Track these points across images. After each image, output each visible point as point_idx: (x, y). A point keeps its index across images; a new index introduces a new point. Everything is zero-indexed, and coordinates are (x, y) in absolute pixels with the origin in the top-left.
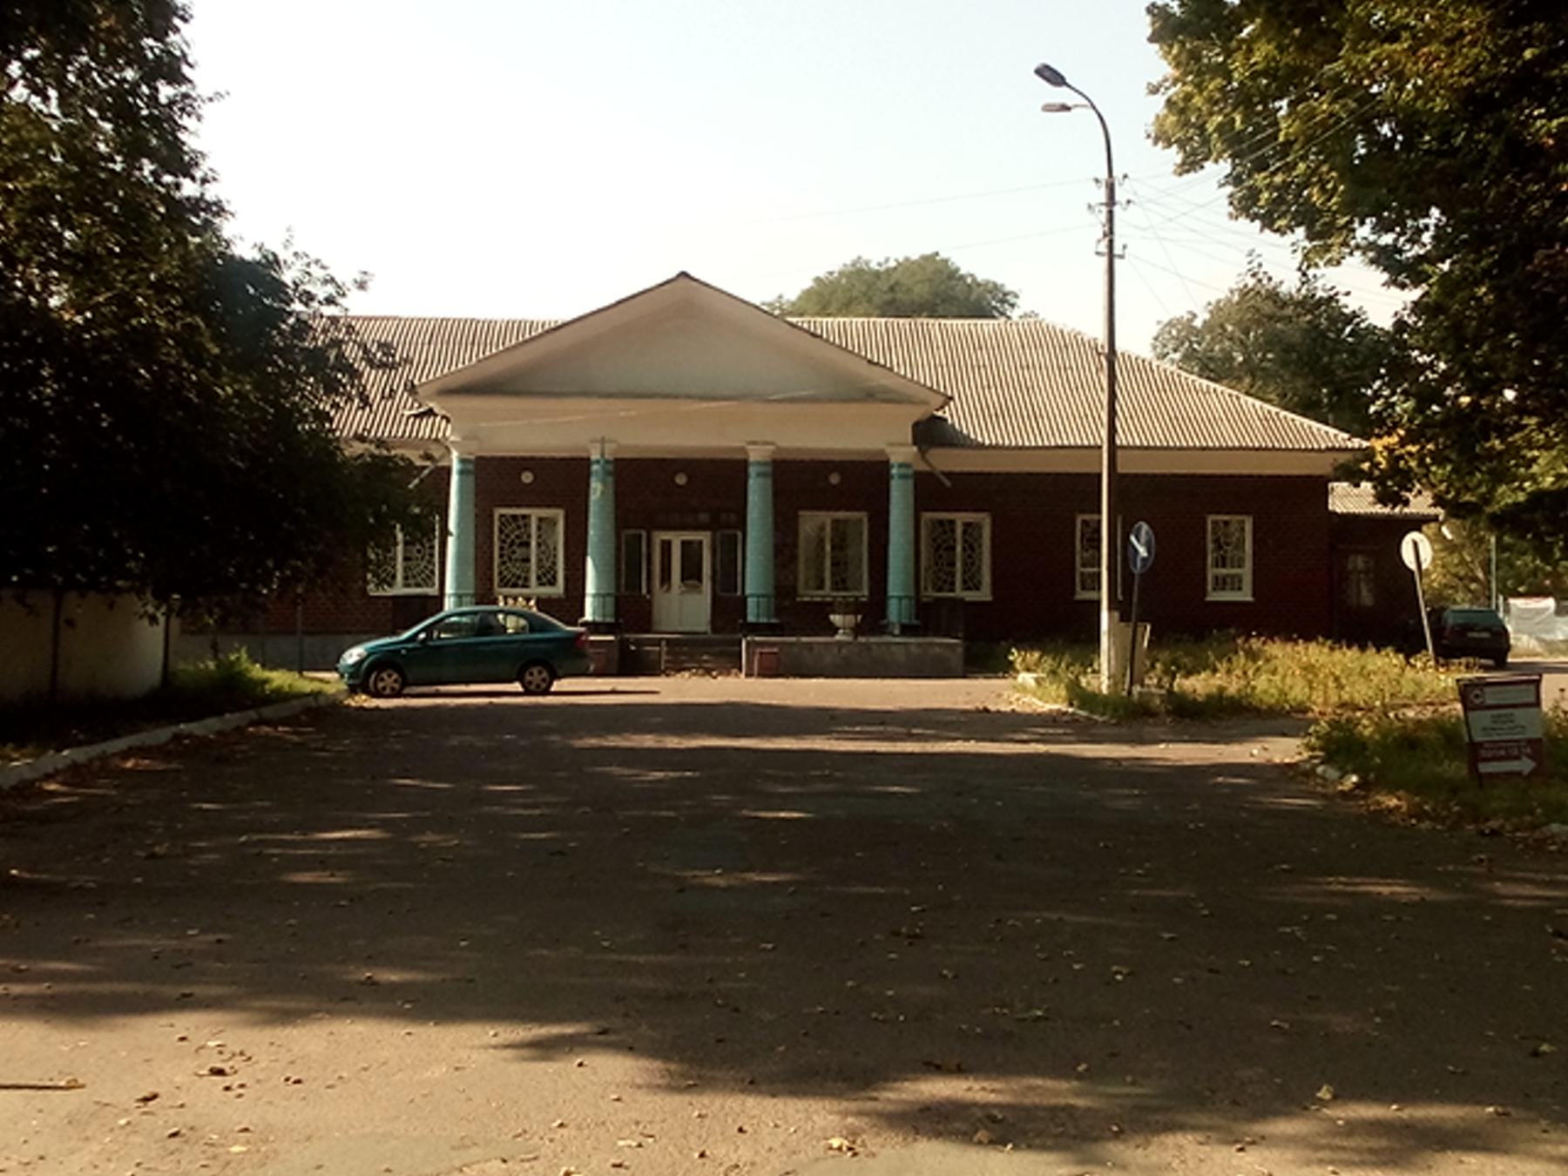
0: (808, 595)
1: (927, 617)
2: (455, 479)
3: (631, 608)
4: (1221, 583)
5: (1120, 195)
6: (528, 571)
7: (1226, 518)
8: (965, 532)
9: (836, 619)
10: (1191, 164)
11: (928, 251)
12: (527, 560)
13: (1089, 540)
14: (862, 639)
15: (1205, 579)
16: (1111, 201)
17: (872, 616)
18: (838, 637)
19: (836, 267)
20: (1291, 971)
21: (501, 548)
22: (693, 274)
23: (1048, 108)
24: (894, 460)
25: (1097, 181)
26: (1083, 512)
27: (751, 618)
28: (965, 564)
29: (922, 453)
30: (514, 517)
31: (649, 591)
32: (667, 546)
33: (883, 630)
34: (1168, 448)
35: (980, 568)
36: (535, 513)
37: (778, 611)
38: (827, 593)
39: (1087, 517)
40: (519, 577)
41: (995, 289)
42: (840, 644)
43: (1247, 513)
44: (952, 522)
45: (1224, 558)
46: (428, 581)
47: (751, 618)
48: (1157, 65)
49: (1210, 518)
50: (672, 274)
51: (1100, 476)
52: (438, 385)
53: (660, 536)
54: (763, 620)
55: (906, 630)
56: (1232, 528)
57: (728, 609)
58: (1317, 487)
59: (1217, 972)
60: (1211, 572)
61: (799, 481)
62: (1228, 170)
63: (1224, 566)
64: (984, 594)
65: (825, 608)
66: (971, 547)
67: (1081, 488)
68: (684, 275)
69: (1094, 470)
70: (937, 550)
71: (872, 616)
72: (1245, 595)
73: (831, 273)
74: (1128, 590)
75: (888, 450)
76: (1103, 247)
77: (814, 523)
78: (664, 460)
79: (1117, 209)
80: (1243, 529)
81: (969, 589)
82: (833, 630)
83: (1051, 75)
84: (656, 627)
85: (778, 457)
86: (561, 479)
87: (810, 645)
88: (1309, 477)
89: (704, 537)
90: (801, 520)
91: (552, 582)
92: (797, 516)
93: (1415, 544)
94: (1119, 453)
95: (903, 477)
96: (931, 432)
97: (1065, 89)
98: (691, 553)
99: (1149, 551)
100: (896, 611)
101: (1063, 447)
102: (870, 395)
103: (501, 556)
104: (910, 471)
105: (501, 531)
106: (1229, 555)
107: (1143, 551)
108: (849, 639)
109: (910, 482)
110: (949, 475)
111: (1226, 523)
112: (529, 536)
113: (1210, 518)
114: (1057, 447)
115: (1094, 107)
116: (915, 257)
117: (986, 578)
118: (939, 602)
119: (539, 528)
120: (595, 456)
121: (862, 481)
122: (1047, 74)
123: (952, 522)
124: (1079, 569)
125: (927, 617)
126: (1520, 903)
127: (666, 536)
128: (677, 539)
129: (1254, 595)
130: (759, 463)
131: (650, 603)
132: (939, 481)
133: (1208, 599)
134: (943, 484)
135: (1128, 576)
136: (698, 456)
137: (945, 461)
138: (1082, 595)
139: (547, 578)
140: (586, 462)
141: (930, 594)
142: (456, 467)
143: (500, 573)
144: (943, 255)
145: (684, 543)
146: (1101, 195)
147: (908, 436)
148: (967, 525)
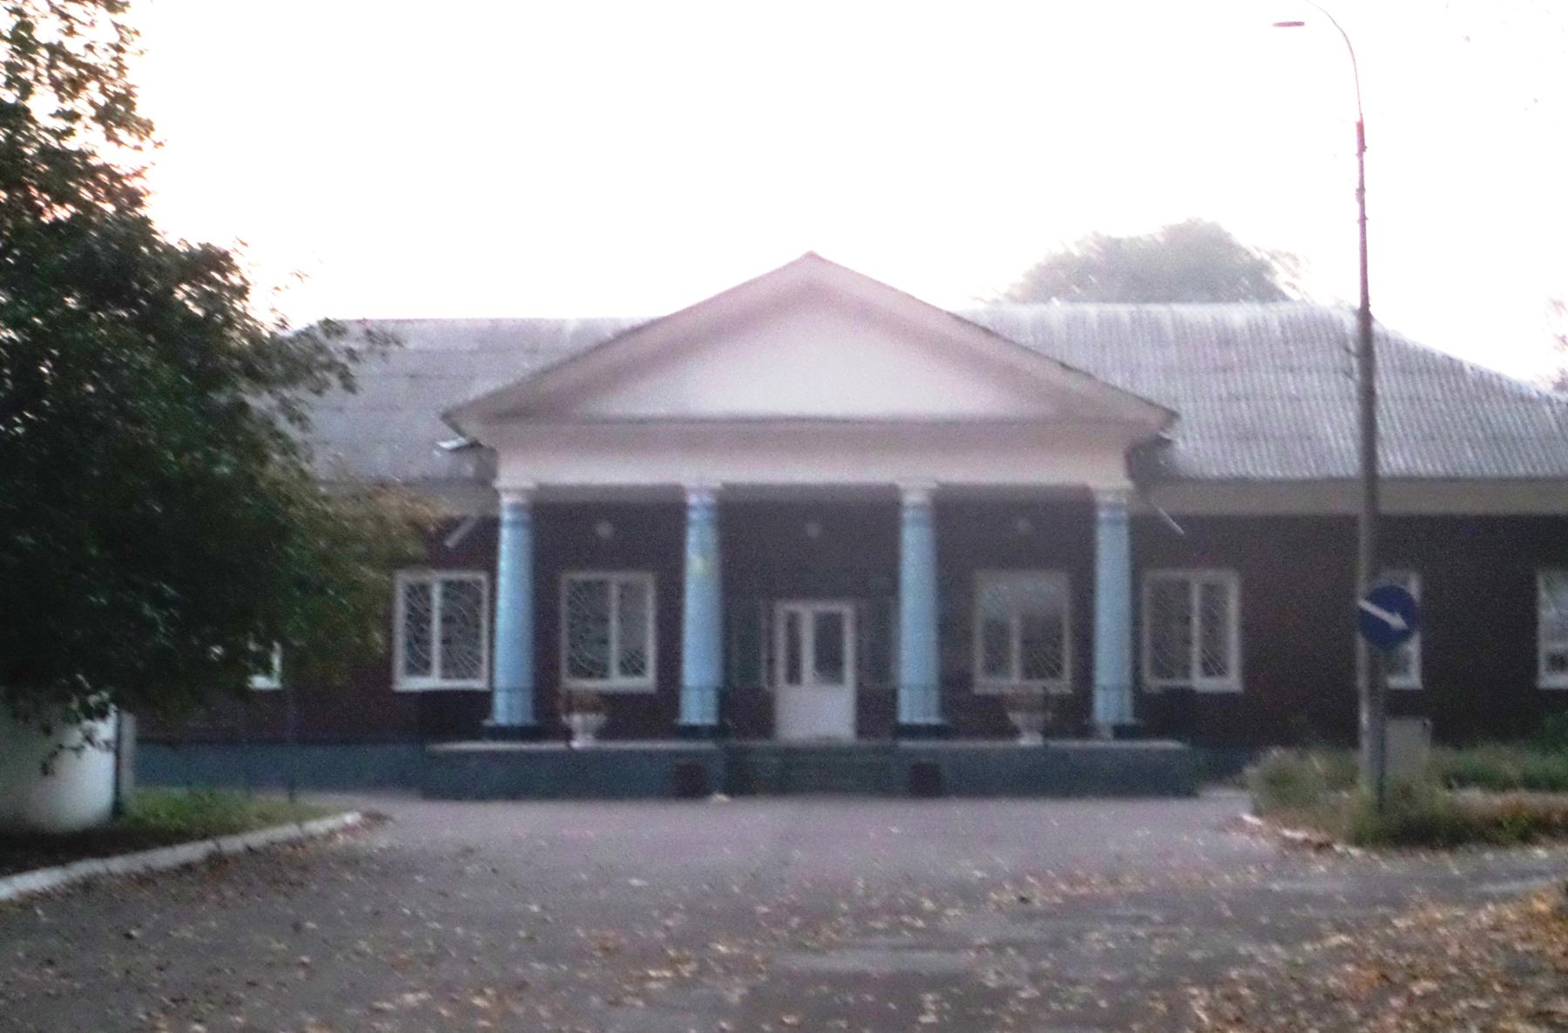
0: (985, 684)
1: (1162, 711)
2: (506, 534)
9: (1017, 718)
11: (1141, 212)
30: (587, 584)
31: (771, 682)
32: (793, 623)
37: (945, 707)
46: (472, 673)
53: (783, 608)
57: (875, 707)
61: (979, 532)
64: (1232, 682)
66: (1213, 620)
68: (811, 256)
77: (1009, 595)
82: (568, 734)
86: (647, 528)
89: (846, 610)
91: (1055, 671)
95: (1114, 522)
96: (1147, 456)
98: (829, 632)
100: (1110, 705)
109: (1124, 531)
110: (1185, 520)
117: (1234, 658)
118: (1170, 693)
126: (1147, 620)
127: (792, 607)
128: (807, 613)
132: (1166, 526)
139: (633, 665)
141: (1153, 683)
142: (506, 516)
143: (571, 659)
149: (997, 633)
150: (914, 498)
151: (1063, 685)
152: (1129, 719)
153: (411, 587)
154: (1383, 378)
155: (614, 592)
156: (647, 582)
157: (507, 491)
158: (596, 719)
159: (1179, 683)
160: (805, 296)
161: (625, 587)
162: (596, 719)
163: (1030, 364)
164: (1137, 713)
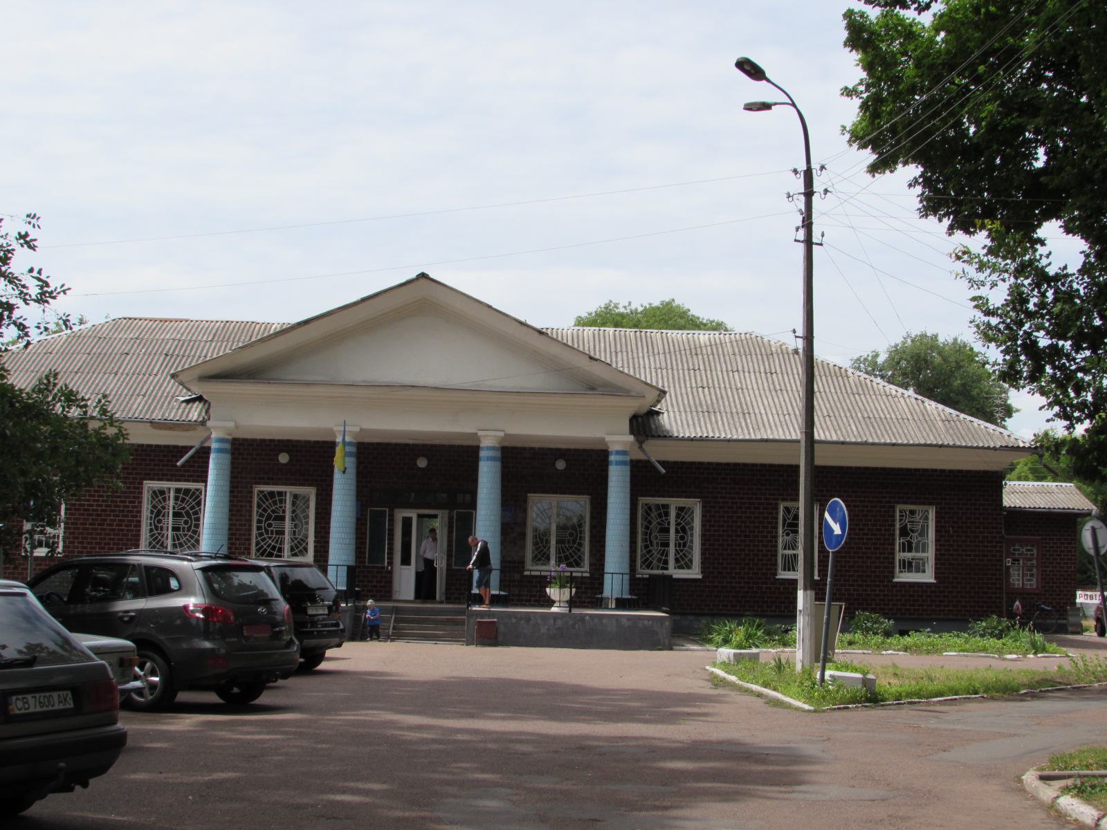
0: (533, 569)
1: (644, 591)
3: (368, 577)
4: (908, 566)
5: (818, 186)
6: (282, 542)
7: (913, 507)
8: (678, 516)
10: (882, 165)
12: (283, 533)
13: (790, 525)
14: (576, 611)
15: (893, 563)
16: (809, 194)
17: (588, 591)
18: (554, 609)
21: (259, 521)
22: (432, 276)
23: (750, 107)
24: (613, 448)
25: (795, 171)
26: (784, 500)
28: (678, 545)
29: (640, 443)
30: (272, 494)
31: (390, 563)
32: (407, 522)
33: (599, 603)
34: (866, 443)
35: (691, 547)
36: (289, 490)
39: (789, 504)
40: (274, 548)
42: (555, 615)
43: (930, 504)
44: (666, 507)
45: (910, 543)
49: (898, 507)
50: (413, 276)
51: (798, 467)
52: (198, 372)
55: (621, 604)
56: (917, 517)
58: (992, 482)
59: (886, 799)
60: (900, 556)
61: (528, 468)
62: (920, 192)
63: (910, 550)
64: (695, 573)
65: (544, 582)
66: (683, 530)
68: (423, 276)
69: (793, 462)
70: (648, 533)
71: (588, 591)
72: (928, 577)
73: (590, 314)
74: (823, 572)
75: (608, 438)
76: (801, 235)
77: (548, 510)
78: (407, 445)
79: (815, 198)
80: (927, 518)
81: (681, 567)
82: (550, 603)
83: (751, 69)
84: (396, 597)
85: (507, 444)
86: (309, 460)
87: (528, 617)
88: (986, 472)
90: (530, 503)
92: (526, 497)
93: (1094, 530)
94: (816, 445)
95: (619, 463)
96: (644, 424)
97: (764, 82)
99: (843, 528)
100: (614, 584)
101: (767, 441)
102: (593, 387)
103: (259, 528)
104: (628, 458)
105: (259, 506)
106: (914, 541)
107: (837, 529)
108: (566, 610)
109: (628, 468)
110: (664, 463)
111: (912, 512)
112: (284, 511)
113: (898, 507)
114: (762, 440)
115: (794, 105)
116: (656, 303)
119: (294, 504)
120: (339, 439)
121: (582, 469)
122: (747, 67)
123: (666, 507)
124: (781, 552)
125: (644, 591)
129: (936, 578)
130: (489, 448)
131: (391, 572)
132: (654, 467)
133: (896, 580)
134: (659, 472)
135: (823, 553)
136: (437, 442)
137: (656, 452)
138: (784, 575)
140: (332, 445)
141: (643, 573)
143: (257, 544)
144: (677, 302)
145: (796, 581)
146: (799, 185)
147: (626, 426)
148: (681, 509)
149: (541, 540)
150: (489, 442)
151: (584, 570)
152: (627, 596)
153: (154, 492)
154: (819, 380)
155: (289, 499)
156: (311, 492)
157: (215, 428)
158: (566, 594)
159: (666, 572)
160: (420, 303)
161: (295, 497)
162: (566, 594)
163: (566, 355)
164: (631, 591)
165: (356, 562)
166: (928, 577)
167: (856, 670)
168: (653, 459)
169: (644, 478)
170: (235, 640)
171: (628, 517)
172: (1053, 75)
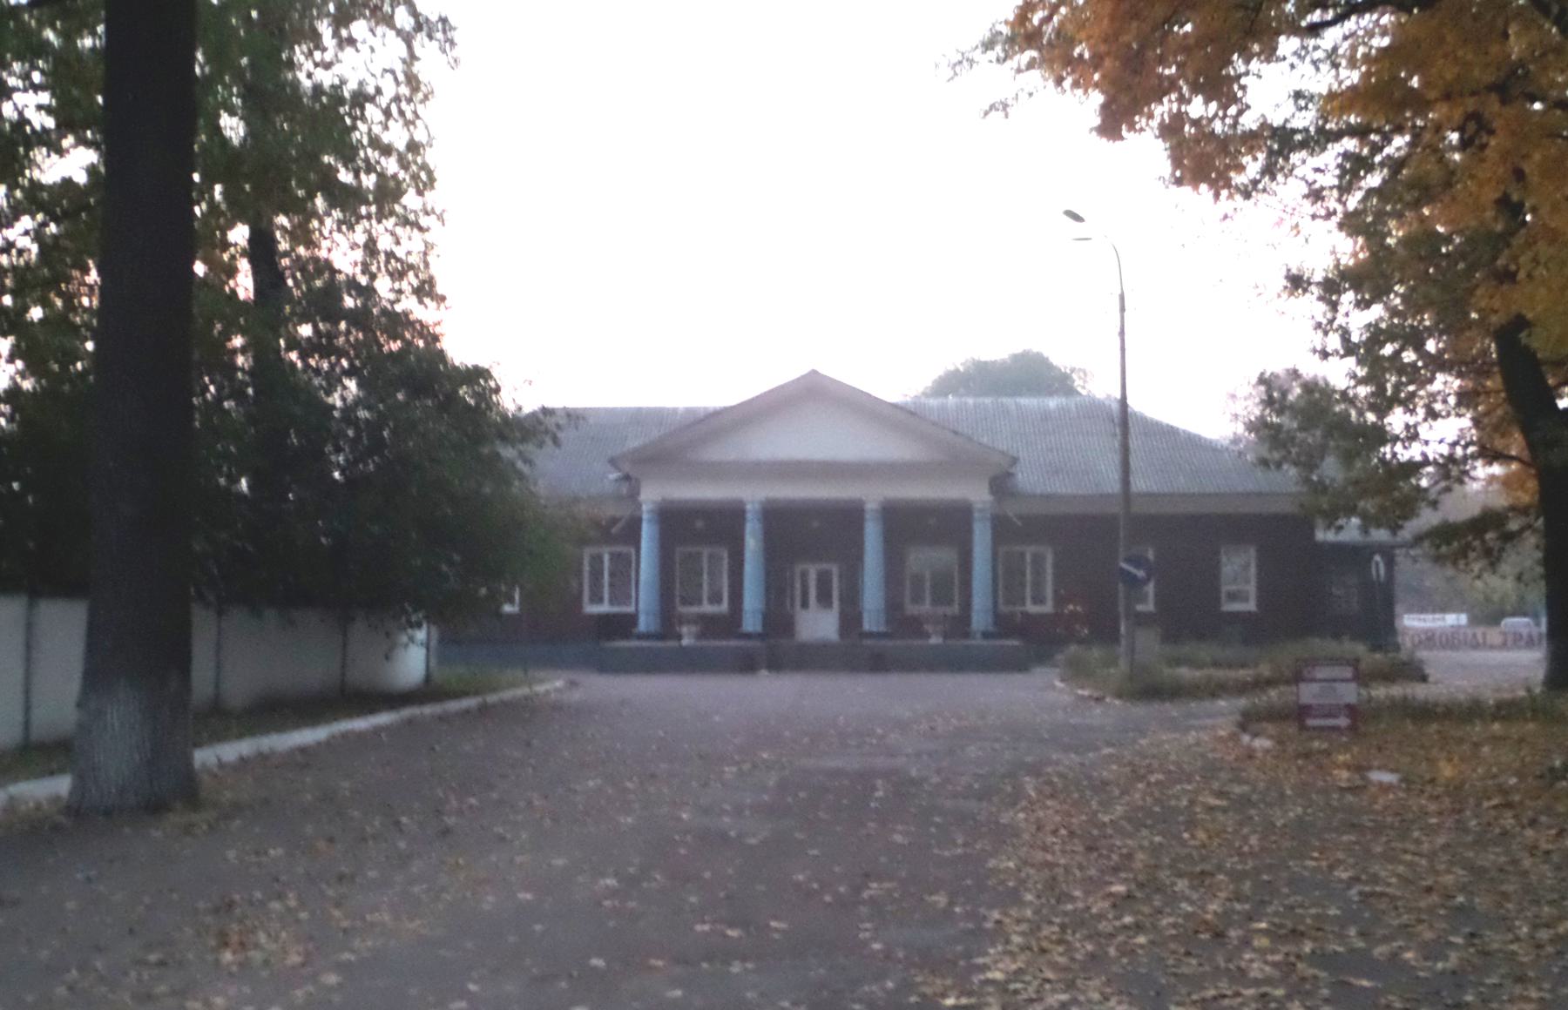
0: (912, 609)
1: (1004, 625)
4: (1233, 597)
14: (950, 642)
19: (899, 373)
20: (283, 878)
27: (866, 627)
31: (792, 605)
33: (967, 635)
38: (926, 607)
41: (476, 368)
46: (627, 603)
47: (866, 627)
48: (58, 179)
54: (875, 629)
61: (904, 524)
67: (848, 517)
70: (1008, 577)
71: (960, 626)
72: (1251, 606)
77: (925, 559)
96: (1001, 484)
100: (980, 619)
110: (1021, 517)
121: (949, 524)
137: (1011, 509)
139: (715, 598)
149: (918, 580)
150: (871, 506)
151: (955, 609)
152: (991, 628)
160: (813, 394)
165: (888, 622)
166: (1251, 606)
167: (1314, 728)
168: (1010, 514)
169: (1002, 529)
170: (1016, 643)
171: (989, 567)
172: (1412, 89)
